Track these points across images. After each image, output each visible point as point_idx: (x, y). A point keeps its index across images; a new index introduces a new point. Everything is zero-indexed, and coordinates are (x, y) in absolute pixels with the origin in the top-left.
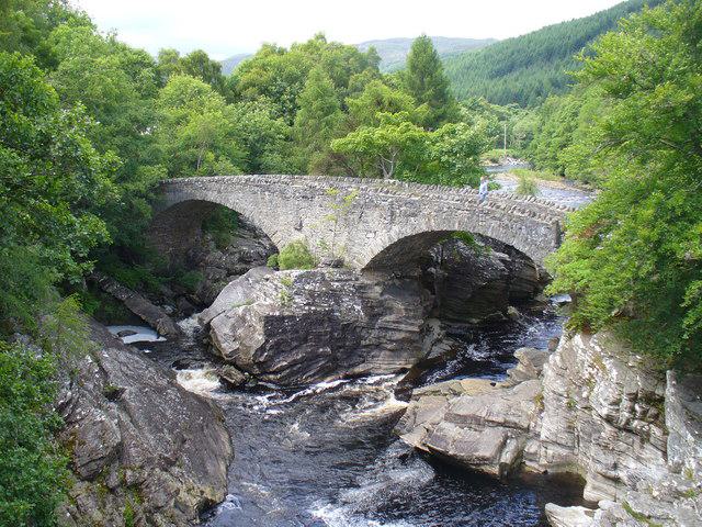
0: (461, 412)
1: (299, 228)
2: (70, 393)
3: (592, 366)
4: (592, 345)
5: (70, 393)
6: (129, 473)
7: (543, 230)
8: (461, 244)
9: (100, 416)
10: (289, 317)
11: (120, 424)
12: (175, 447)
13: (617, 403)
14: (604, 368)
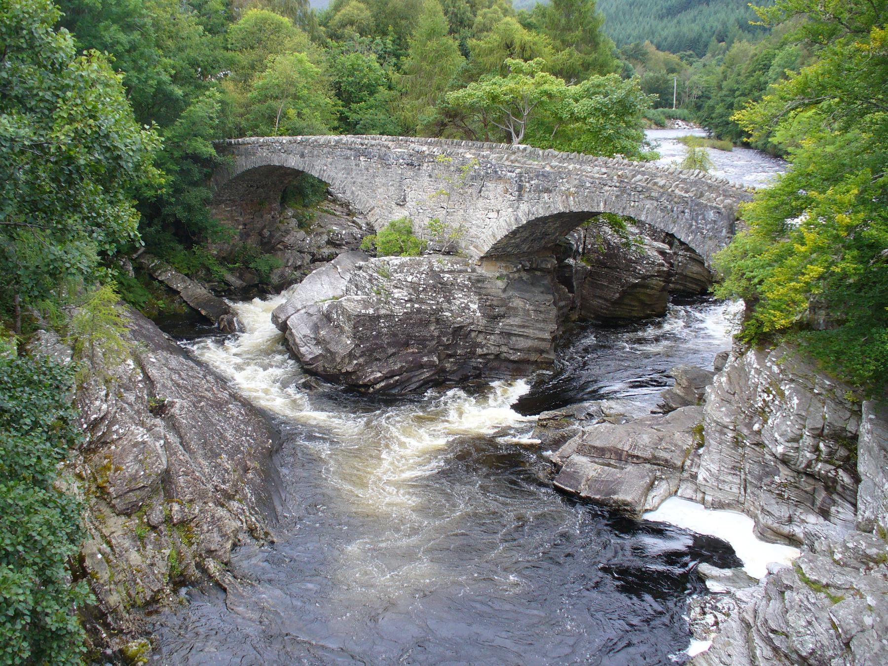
0: (598, 444)
1: (402, 203)
2: (104, 406)
3: (767, 391)
4: (769, 364)
5: (104, 406)
6: (176, 507)
7: (711, 215)
8: (607, 229)
9: (140, 434)
10: (386, 316)
11: (167, 446)
12: (234, 476)
13: (796, 439)
14: (782, 394)
